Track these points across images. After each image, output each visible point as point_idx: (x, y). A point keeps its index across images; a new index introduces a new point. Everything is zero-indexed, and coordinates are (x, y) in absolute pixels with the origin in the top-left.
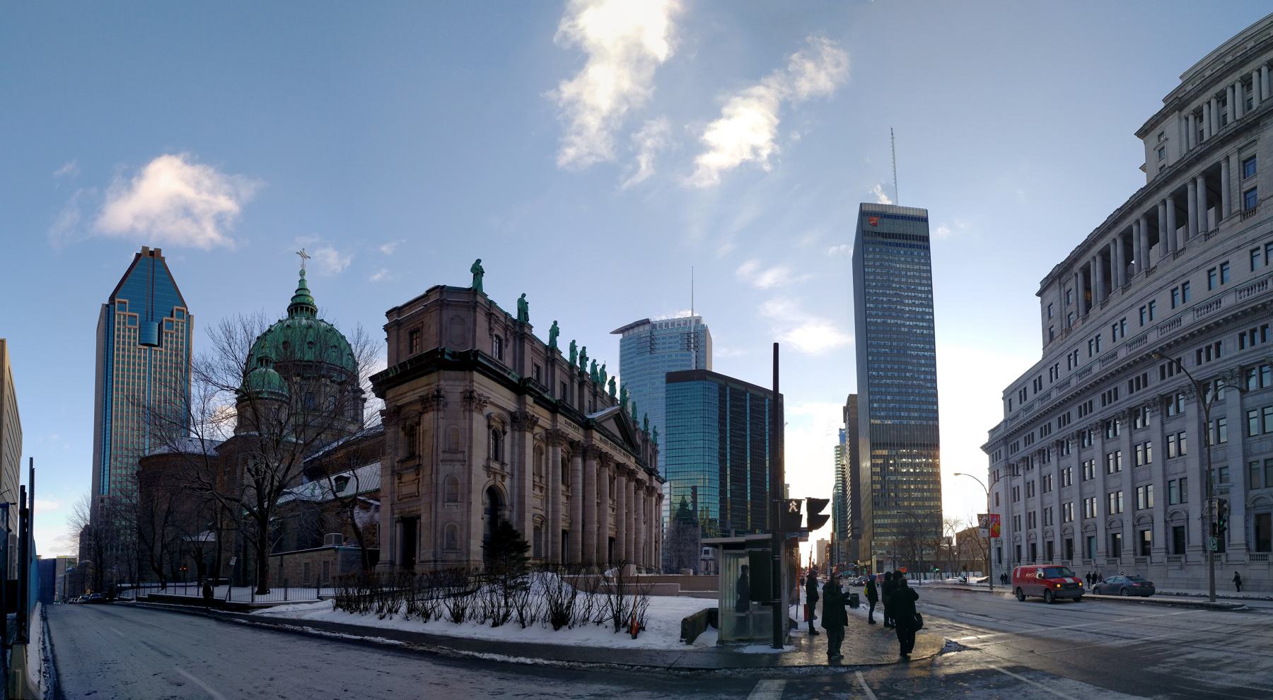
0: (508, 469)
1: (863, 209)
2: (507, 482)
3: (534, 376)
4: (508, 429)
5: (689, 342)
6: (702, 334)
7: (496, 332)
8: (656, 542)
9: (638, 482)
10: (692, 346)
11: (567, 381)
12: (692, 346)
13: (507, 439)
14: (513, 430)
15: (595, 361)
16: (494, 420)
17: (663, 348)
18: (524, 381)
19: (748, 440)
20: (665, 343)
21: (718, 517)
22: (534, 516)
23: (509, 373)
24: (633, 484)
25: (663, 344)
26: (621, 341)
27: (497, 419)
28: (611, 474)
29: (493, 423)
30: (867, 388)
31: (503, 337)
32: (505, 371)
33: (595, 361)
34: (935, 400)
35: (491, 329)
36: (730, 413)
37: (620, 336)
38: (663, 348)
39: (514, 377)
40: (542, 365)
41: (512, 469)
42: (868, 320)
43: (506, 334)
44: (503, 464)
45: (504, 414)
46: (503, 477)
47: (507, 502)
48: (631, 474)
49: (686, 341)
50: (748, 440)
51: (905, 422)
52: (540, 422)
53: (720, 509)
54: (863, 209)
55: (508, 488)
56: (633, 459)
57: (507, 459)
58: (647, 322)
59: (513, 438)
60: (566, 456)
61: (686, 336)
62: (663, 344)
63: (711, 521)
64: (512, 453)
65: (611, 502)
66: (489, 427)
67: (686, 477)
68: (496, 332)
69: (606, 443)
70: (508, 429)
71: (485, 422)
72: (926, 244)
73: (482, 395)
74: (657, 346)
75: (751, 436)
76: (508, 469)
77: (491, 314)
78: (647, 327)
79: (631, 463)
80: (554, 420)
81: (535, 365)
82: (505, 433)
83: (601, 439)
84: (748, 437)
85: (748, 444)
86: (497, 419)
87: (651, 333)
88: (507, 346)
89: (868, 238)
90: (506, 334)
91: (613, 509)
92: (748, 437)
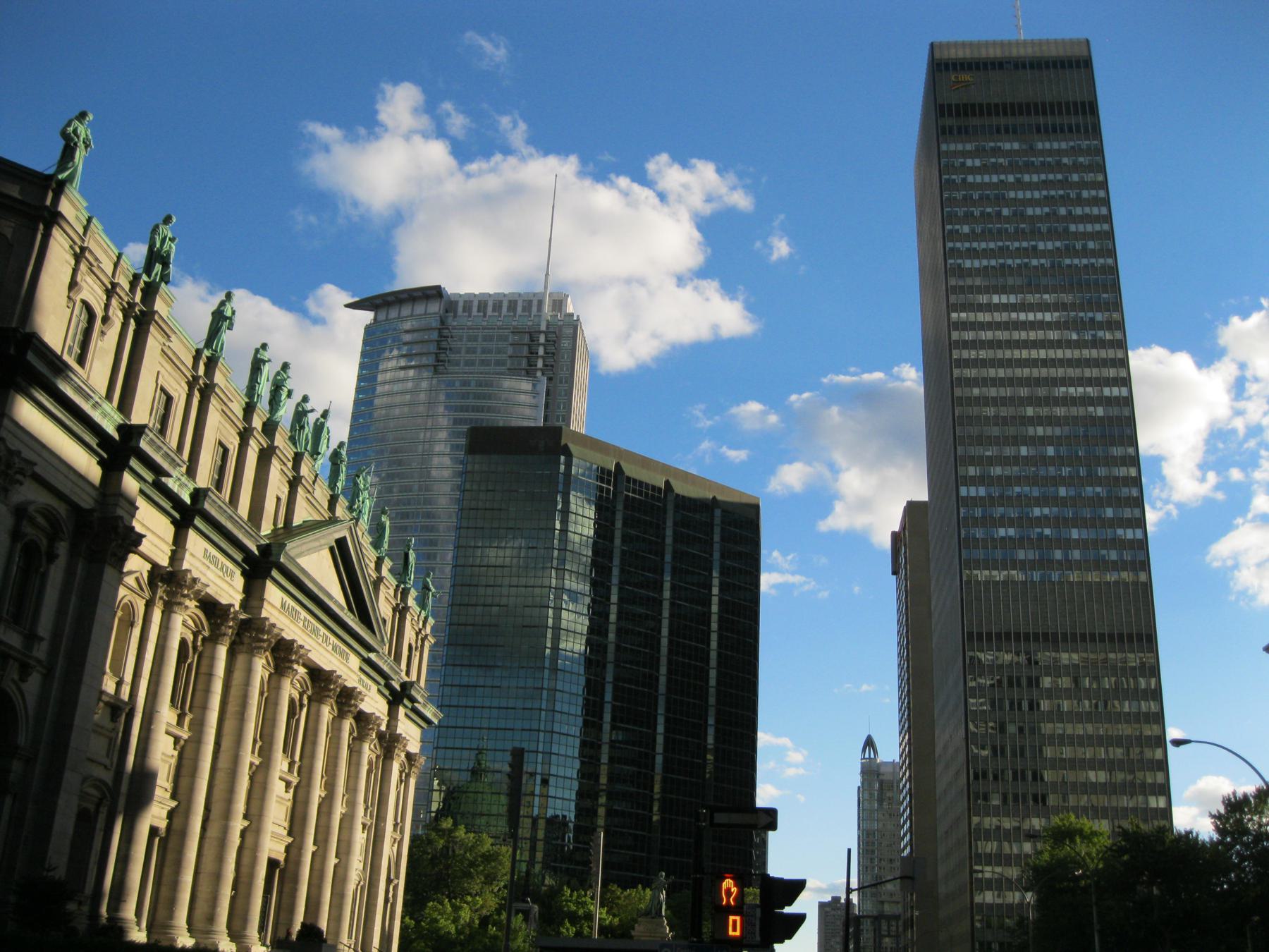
0: (40, 652)
1: (937, 55)
2: (33, 684)
3: (153, 423)
4: (62, 548)
5: (533, 353)
6: (569, 331)
7: (85, 294)
8: (389, 881)
9: (363, 720)
10: (540, 364)
11: (233, 443)
12: (540, 364)
13: (56, 574)
14: (73, 554)
15: (305, 399)
16: (32, 521)
17: (467, 363)
18: (131, 433)
19: (666, 613)
20: (472, 350)
21: (571, 816)
22: (85, 780)
23: (96, 405)
24: (348, 724)
25: (469, 351)
26: (369, 330)
27: (40, 520)
28: (296, 696)
29: (28, 529)
30: (935, 161)
31: (99, 313)
32: (87, 397)
33: (305, 399)
34: (1142, 557)
35: (73, 285)
36: (624, 541)
37: (367, 316)
38: (467, 363)
39: (108, 419)
40: (179, 392)
41: (53, 651)
42: (950, 245)
43: (107, 307)
44: (31, 638)
45: (62, 509)
46: (25, 670)
47: (22, 739)
48: (346, 698)
49: (525, 351)
50: (666, 613)
51: (1055, 576)
52: (144, 547)
53: (580, 794)
54: (937, 55)
55: (31, 701)
56: (355, 661)
57: (45, 625)
58: (435, 293)
59: (70, 572)
60: (190, 637)
61: (526, 339)
62: (469, 351)
63: (552, 821)
64: (61, 611)
65: (285, 767)
66: (16, 535)
67: (495, 703)
68: (85, 294)
69: (294, 617)
70: (62, 548)
71: (9, 522)
72: (1147, 657)
73: (19, 453)
74: (453, 357)
75: (672, 604)
76: (40, 652)
77: (83, 249)
78: (435, 307)
79: (348, 669)
80: (179, 541)
81: (163, 390)
82: (52, 557)
83: (283, 605)
84: (666, 605)
85: (665, 623)
86: (40, 520)
87: (442, 322)
88: (103, 333)
89: (949, 122)
90: (107, 307)
91: (288, 784)
92: (666, 605)
